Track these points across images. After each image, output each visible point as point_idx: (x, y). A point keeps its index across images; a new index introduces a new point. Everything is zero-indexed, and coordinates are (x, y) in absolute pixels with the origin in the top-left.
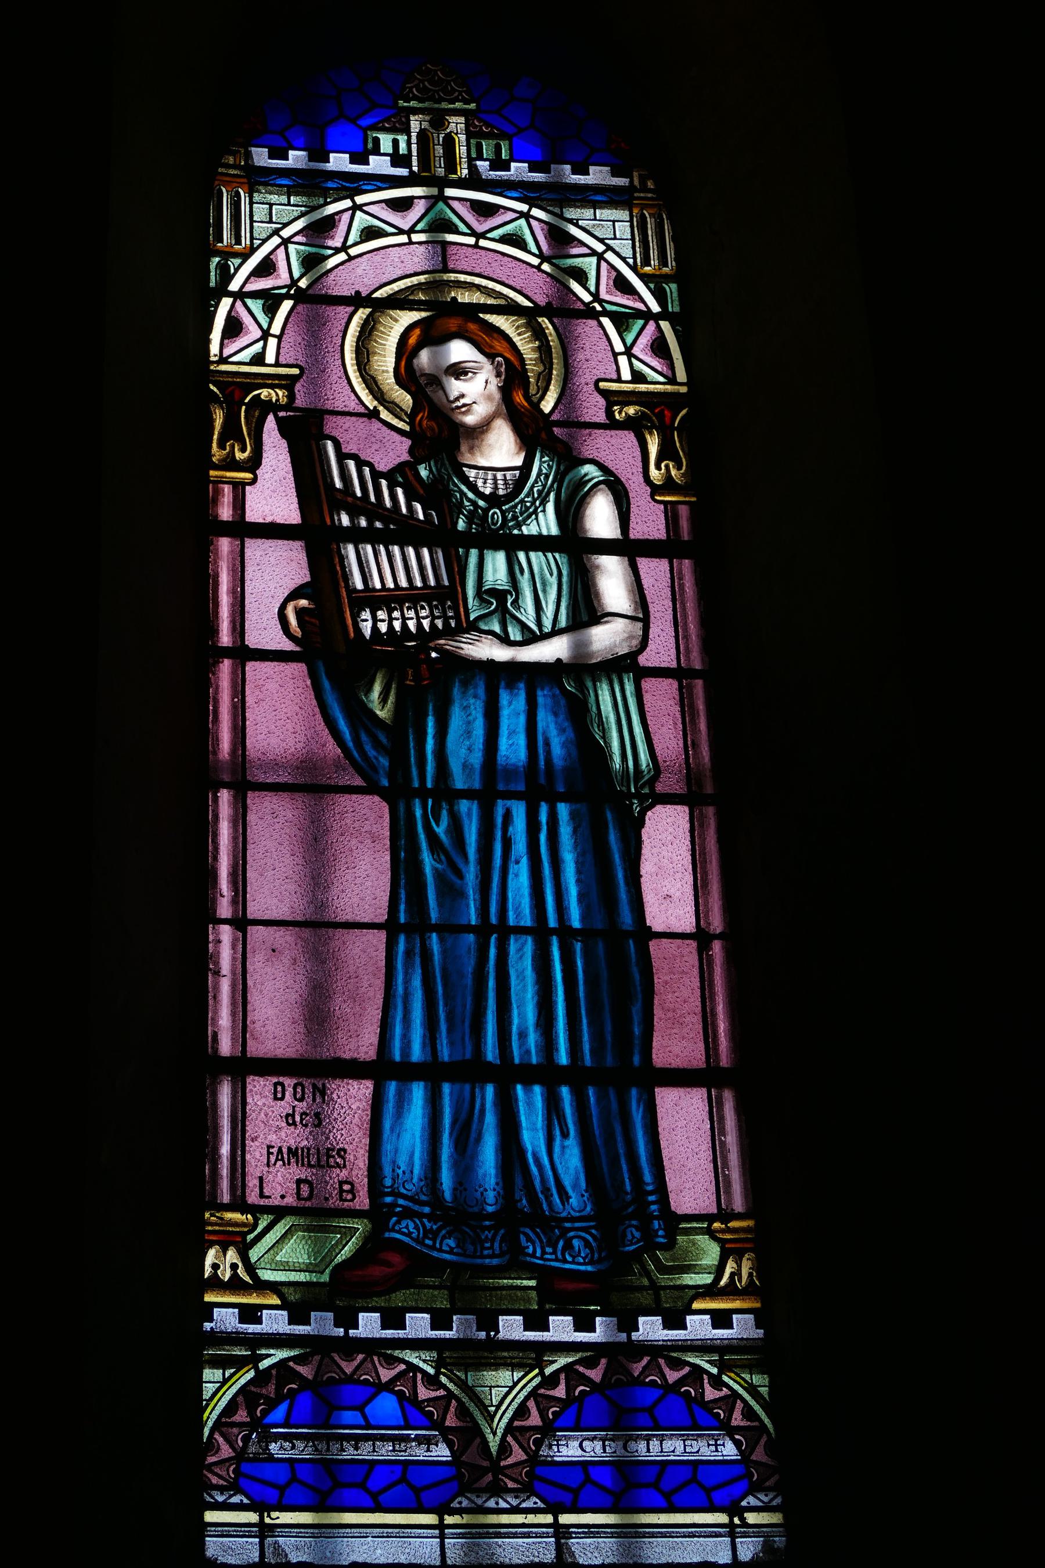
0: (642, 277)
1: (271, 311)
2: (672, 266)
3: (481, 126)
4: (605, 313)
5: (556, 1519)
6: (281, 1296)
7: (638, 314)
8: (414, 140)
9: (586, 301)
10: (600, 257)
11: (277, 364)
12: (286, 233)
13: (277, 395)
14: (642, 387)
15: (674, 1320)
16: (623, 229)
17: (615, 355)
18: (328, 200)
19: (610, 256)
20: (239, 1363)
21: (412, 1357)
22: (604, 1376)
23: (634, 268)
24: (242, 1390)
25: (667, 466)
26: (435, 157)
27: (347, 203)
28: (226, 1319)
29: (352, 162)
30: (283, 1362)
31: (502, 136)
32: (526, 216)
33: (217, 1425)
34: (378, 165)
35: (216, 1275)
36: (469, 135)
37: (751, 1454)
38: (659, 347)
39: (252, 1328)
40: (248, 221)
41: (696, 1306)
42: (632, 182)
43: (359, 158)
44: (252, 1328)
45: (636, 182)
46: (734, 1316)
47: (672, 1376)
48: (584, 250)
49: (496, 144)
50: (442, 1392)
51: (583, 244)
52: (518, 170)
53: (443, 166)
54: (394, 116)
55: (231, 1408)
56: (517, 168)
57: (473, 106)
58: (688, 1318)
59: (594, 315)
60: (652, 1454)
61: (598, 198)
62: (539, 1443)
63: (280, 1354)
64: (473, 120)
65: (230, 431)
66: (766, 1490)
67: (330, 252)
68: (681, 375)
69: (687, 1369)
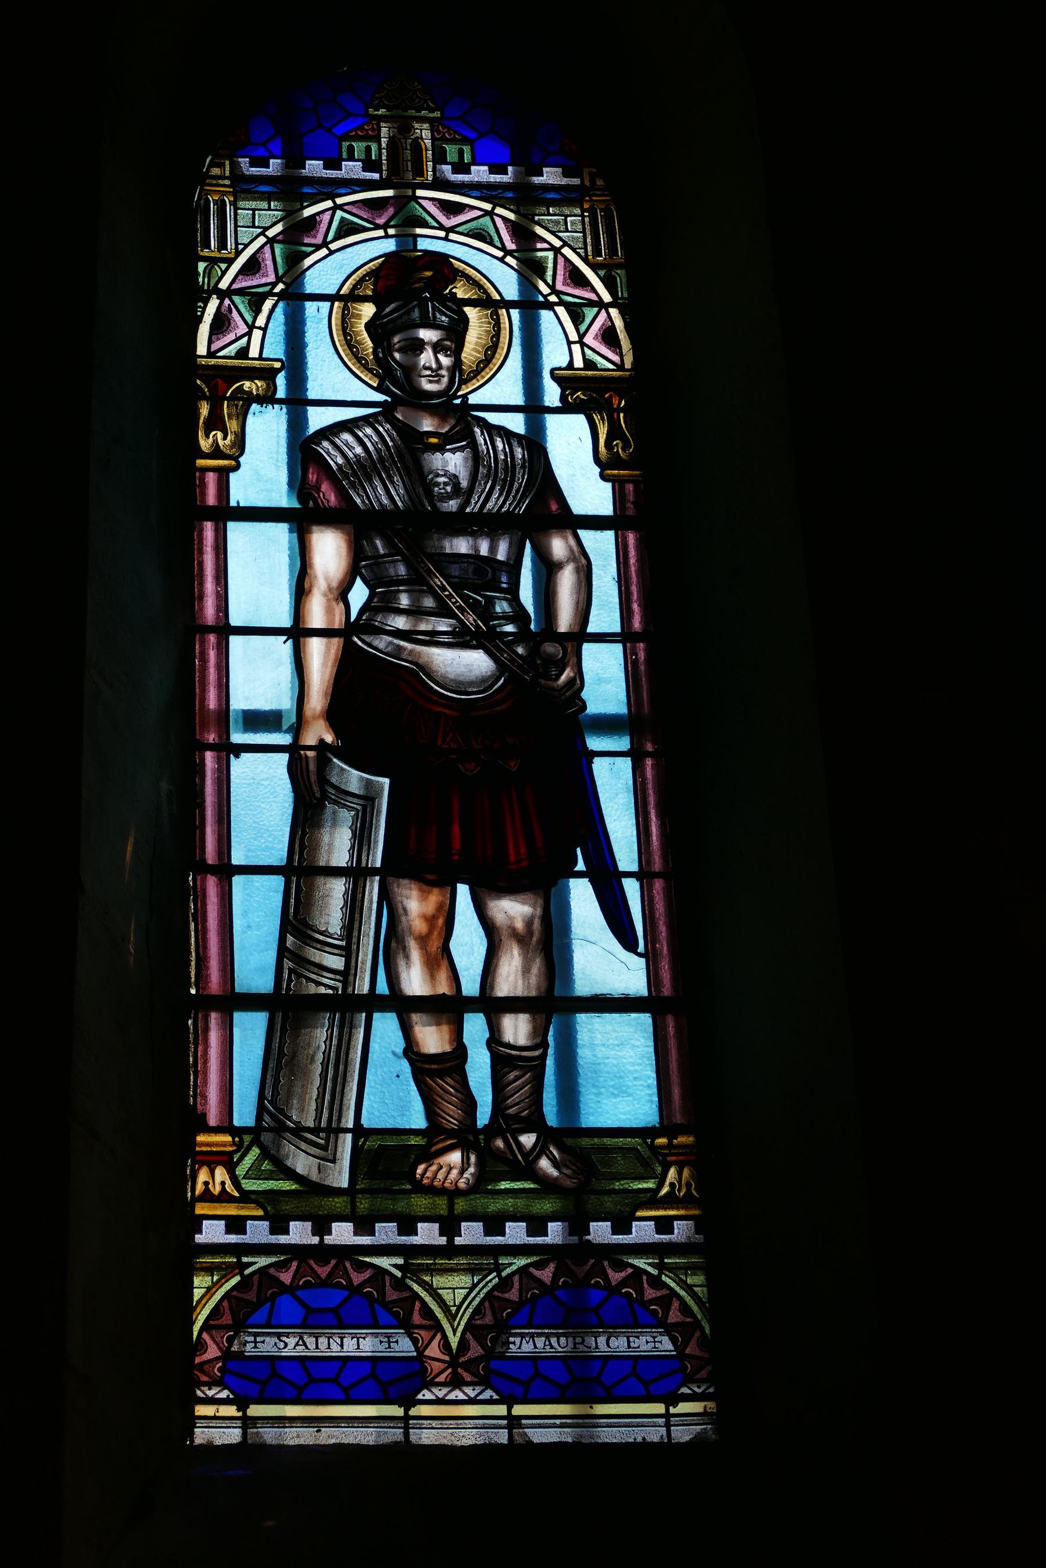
0: (594, 267)
1: (256, 308)
3: (444, 133)
4: (561, 303)
5: (509, 1410)
6: (264, 1209)
7: (591, 304)
8: (384, 145)
10: (557, 251)
11: (260, 358)
12: (271, 233)
15: (622, 1226)
17: (569, 343)
18: (305, 204)
19: (566, 251)
20: (227, 1271)
21: (641, 1263)
22: (294, 1278)
23: (585, 260)
24: (227, 1295)
26: (403, 161)
27: (329, 204)
28: (212, 1233)
29: (325, 168)
30: (263, 1270)
31: (465, 141)
32: (490, 214)
33: (205, 1327)
34: (352, 169)
35: (207, 1190)
36: (433, 139)
37: (686, 1347)
38: (609, 336)
40: (233, 226)
43: (334, 163)
45: (587, 183)
46: (675, 1223)
47: (357, 1278)
48: (546, 246)
49: (348, 146)
50: (665, 1292)
51: (545, 241)
52: (480, 173)
54: (367, 124)
55: (215, 1312)
56: (274, 164)
57: (437, 114)
58: (634, 1224)
59: (549, 306)
61: (552, 195)
62: (230, 1340)
63: (521, 1262)
64: (438, 126)
66: (699, 1382)
67: (311, 249)
68: (628, 365)
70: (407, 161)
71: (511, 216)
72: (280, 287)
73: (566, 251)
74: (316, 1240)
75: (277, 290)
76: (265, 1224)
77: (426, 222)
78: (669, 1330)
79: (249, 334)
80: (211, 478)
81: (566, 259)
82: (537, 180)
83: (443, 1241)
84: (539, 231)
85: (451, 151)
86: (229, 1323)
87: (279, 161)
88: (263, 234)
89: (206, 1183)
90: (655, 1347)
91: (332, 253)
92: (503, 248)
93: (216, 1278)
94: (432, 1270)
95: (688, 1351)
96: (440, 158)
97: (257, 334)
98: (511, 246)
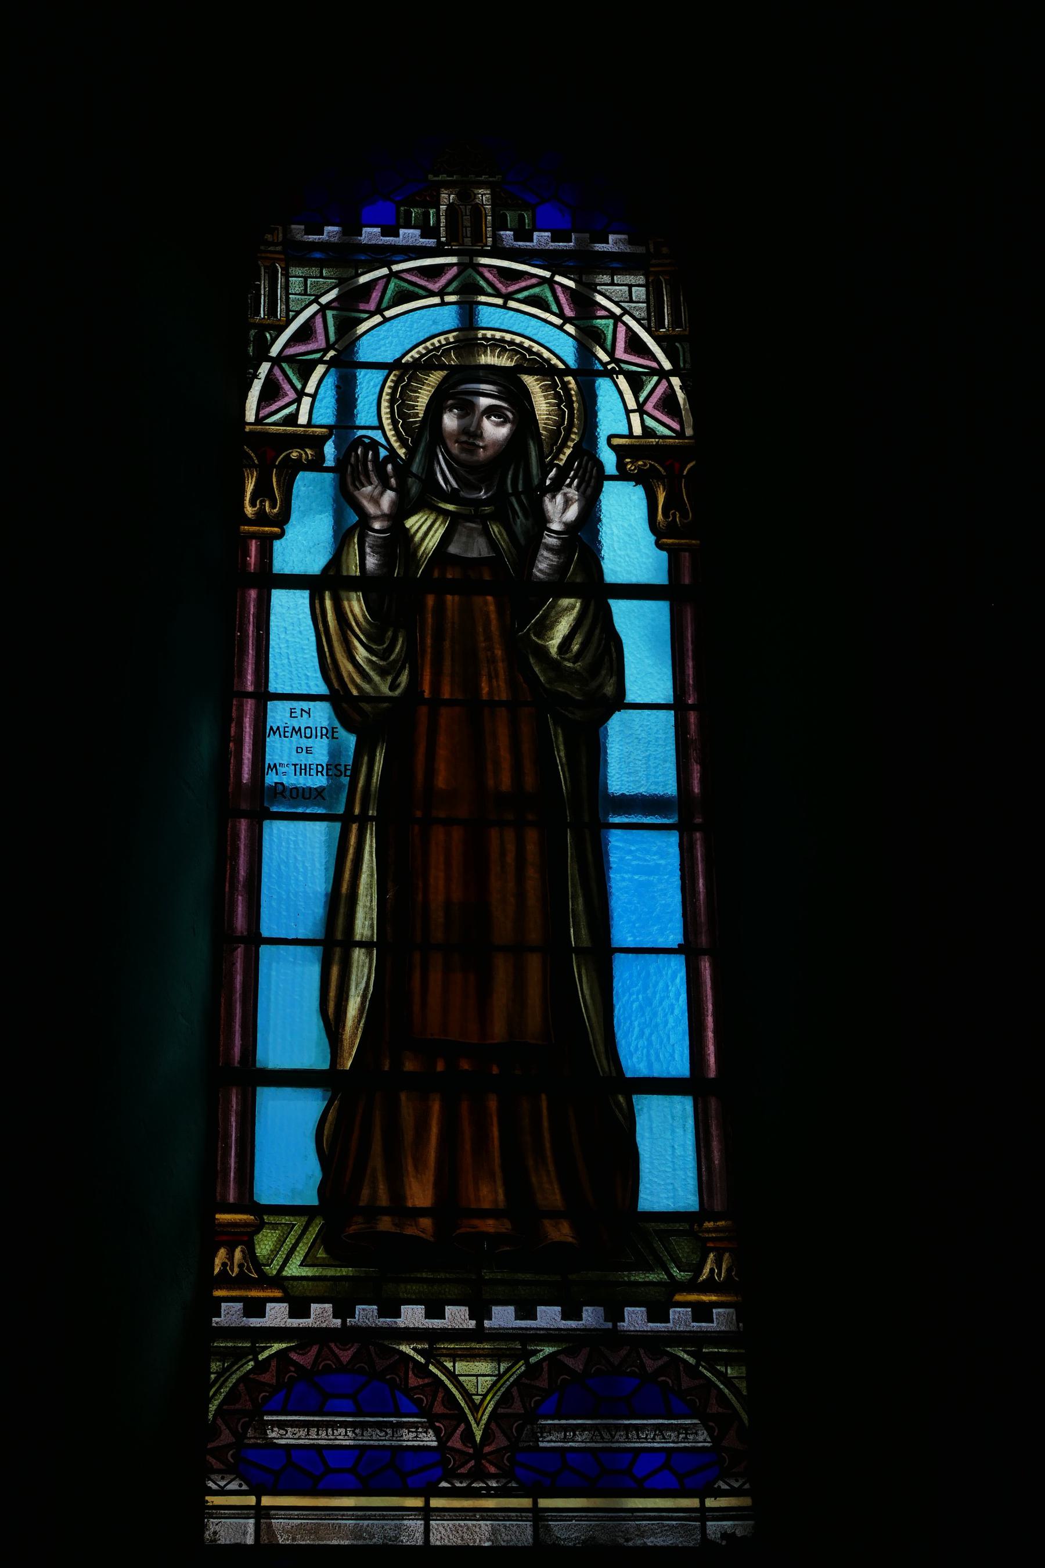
2: (686, 327)
4: (622, 372)
7: (653, 372)
9: (604, 361)
10: (617, 319)
11: (309, 424)
12: (324, 300)
13: (306, 453)
14: (653, 441)
15: (658, 1314)
16: (640, 293)
17: (628, 412)
19: (626, 318)
25: (674, 515)
26: (463, 227)
27: (384, 271)
28: (230, 1314)
30: (279, 1352)
32: (550, 282)
39: (255, 1322)
41: (678, 1298)
42: (648, 249)
44: (255, 1322)
52: (541, 239)
53: (469, 235)
55: (232, 1396)
59: (609, 374)
60: (364, 1438)
61: (317, 255)
65: (263, 491)
68: (689, 432)
69: (666, 1359)
70: (466, 227)
71: (571, 284)
72: (332, 353)
73: (626, 318)
74: (338, 1322)
75: (327, 358)
76: (284, 1307)
77: (482, 288)
78: (706, 1420)
79: (298, 401)
80: (253, 546)
81: (629, 328)
82: (600, 247)
83: (472, 1324)
84: (599, 299)
85: (510, 217)
86: (520, 1412)
87: (336, 229)
88: (316, 301)
89: (224, 1265)
90: (417, 1437)
91: (386, 320)
92: (561, 315)
93: (503, 1366)
94: (454, 1357)
95: (725, 1443)
96: (500, 224)
97: (306, 401)
98: (569, 313)
